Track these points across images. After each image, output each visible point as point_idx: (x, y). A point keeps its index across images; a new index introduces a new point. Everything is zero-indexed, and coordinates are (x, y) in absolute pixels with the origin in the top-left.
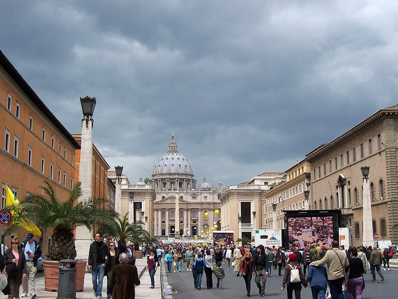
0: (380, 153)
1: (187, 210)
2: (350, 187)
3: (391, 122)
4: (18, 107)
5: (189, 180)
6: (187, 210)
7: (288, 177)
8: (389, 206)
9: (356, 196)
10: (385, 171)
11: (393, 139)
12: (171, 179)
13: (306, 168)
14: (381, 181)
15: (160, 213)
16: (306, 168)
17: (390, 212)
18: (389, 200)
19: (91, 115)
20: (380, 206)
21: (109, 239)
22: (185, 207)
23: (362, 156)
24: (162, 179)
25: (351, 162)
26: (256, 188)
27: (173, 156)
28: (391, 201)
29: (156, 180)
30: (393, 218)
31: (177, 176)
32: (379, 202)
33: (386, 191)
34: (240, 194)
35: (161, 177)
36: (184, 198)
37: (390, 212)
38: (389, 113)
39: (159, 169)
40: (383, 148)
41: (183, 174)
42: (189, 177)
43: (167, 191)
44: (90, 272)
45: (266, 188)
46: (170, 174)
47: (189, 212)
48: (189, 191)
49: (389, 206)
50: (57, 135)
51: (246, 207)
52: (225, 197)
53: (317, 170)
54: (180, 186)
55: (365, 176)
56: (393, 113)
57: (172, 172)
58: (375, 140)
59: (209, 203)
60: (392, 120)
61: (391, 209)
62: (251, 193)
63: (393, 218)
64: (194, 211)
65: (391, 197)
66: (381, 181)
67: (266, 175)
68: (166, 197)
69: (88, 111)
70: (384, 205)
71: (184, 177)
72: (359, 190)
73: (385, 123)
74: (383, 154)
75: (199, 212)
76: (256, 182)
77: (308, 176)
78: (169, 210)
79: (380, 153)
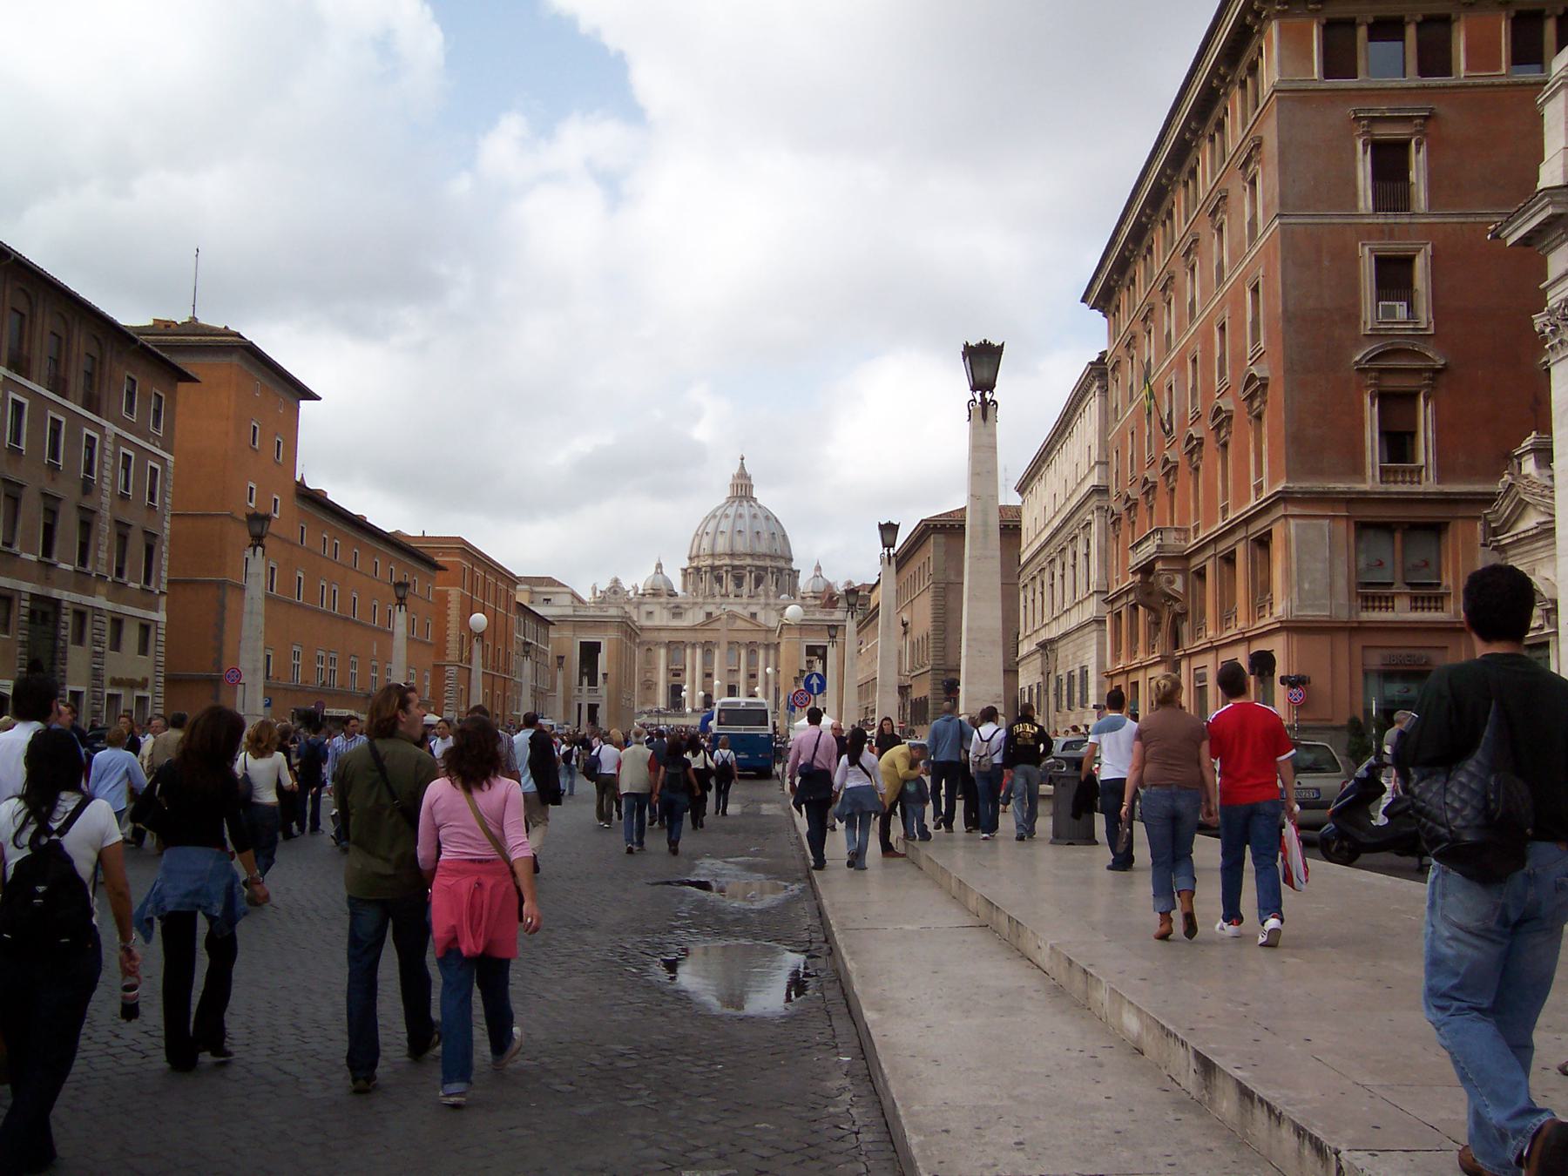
1: (767, 647)
5: (780, 570)
6: (694, 646)
15: (699, 652)
19: (991, 387)
21: (427, 732)
22: (759, 638)
27: (741, 510)
29: (698, 569)
31: (749, 561)
36: (761, 618)
41: (765, 555)
42: (781, 564)
43: (718, 599)
44: (1406, 845)
46: (752, 555)
47: (772, 652)
48: (772, 601)
51: (590, 652)
54: (739, 585)
59: (659, 629)
68: (716, 613)
69: (985, 374)
71: (768, 563)
78: (669, 645)
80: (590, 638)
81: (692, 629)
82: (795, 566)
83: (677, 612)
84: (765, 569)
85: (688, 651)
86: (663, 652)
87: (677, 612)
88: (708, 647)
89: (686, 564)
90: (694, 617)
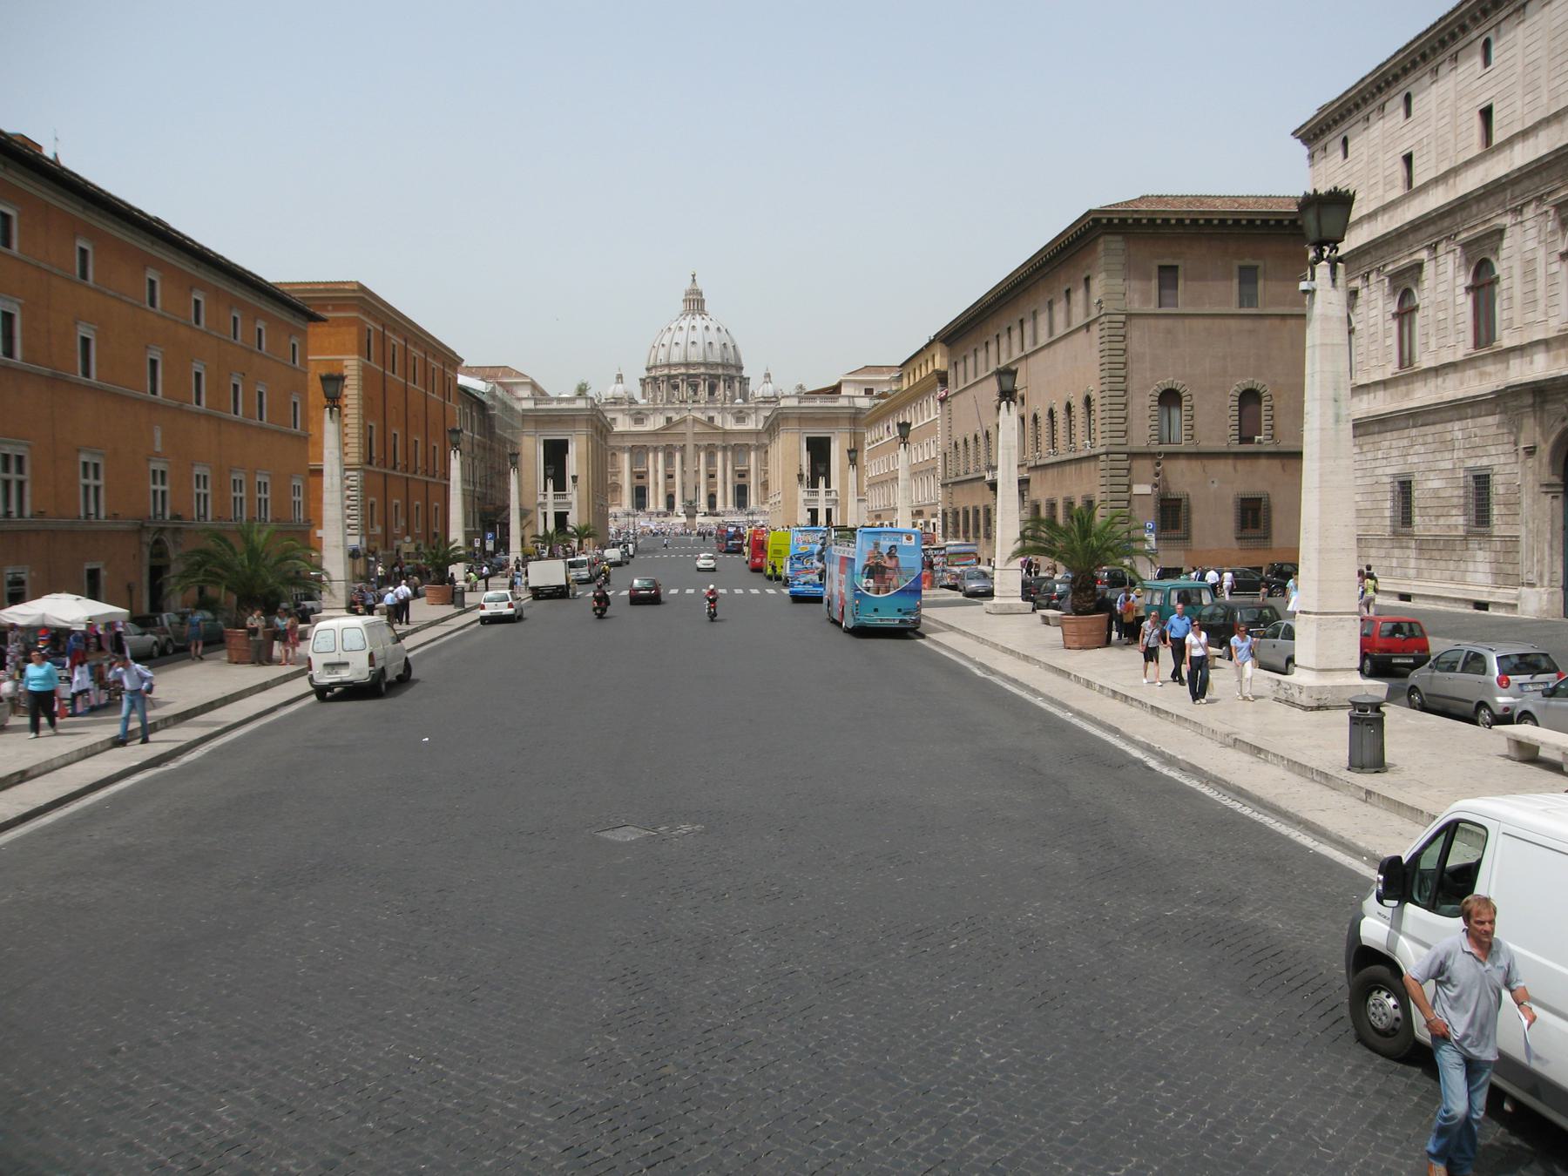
0: (1087, 326)
1: (725, 449)
2: (1024, 410)
3: (1115, 243)
4: (83, 252)
5: (732, 378)
7: (905, 380)
8: (1102, 465)
9: (988, 449)
10: (1098, 374)
11: (1121, 289)
12: (689, 376)
13: (939, 362)
14: (1088, 401)
15: (660, 455)
16: (939, 362)
17: (1103, 481)
18: (1103, 450)
20: (1085, 465)
23: (1051, 333)
24: (670, 377)
25: (1028, 349)
26: (842, 402)
28: (1107, 454)
29: (655, 379)
30: (1110, 496)
31: (702, 370)
32: (1084, 454)
33: (1098, 426)
34: (803, 418)
35: (666, 371)
36: (718, 421)
37: (1103, 481)
38: (1110, 220)
39: (662, 356)
40: (1094, 313)
41: (718, 365)
42: (733, 372)
45: (864, 403)
49: (1102, 465)
50: (1167, 204)
52: (774, 425)
53: (960, 367)
54: (711, 393)
55: (1008, 395)
56: (1121, 220)
57: (693, 358)
58: (1079, 296)
60: (1120, 238)
61: (1107, 473)
62: (831, 418)
63: (1110, 496)
64: (740, 450)
65: (1107, 441)
66: (1088, 401)
67: (870, 373)
68: (676, 417)
70: (1092, 464)
72: (992, 437)
73: (1101, 248)
74: (1095, 328)
75: (753, 454)
76: (845, 391)
77: (942, 378)
79: (1087, 326)
80: (556, 435)
81: (654, 434)
82: (745, 373)
83: (639, 417)
84: (718, 377)
85: (651, 456)
86: (626, 456)
87: (639, 417)
88: (669, 453)
89: (644, 374)
90: (655, 423)
